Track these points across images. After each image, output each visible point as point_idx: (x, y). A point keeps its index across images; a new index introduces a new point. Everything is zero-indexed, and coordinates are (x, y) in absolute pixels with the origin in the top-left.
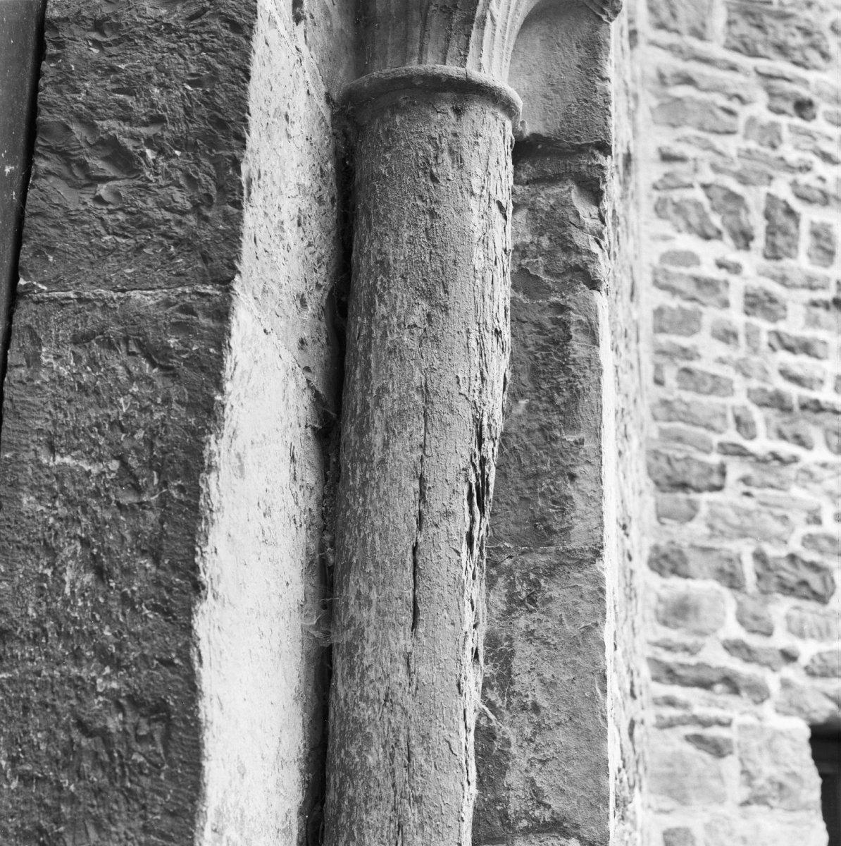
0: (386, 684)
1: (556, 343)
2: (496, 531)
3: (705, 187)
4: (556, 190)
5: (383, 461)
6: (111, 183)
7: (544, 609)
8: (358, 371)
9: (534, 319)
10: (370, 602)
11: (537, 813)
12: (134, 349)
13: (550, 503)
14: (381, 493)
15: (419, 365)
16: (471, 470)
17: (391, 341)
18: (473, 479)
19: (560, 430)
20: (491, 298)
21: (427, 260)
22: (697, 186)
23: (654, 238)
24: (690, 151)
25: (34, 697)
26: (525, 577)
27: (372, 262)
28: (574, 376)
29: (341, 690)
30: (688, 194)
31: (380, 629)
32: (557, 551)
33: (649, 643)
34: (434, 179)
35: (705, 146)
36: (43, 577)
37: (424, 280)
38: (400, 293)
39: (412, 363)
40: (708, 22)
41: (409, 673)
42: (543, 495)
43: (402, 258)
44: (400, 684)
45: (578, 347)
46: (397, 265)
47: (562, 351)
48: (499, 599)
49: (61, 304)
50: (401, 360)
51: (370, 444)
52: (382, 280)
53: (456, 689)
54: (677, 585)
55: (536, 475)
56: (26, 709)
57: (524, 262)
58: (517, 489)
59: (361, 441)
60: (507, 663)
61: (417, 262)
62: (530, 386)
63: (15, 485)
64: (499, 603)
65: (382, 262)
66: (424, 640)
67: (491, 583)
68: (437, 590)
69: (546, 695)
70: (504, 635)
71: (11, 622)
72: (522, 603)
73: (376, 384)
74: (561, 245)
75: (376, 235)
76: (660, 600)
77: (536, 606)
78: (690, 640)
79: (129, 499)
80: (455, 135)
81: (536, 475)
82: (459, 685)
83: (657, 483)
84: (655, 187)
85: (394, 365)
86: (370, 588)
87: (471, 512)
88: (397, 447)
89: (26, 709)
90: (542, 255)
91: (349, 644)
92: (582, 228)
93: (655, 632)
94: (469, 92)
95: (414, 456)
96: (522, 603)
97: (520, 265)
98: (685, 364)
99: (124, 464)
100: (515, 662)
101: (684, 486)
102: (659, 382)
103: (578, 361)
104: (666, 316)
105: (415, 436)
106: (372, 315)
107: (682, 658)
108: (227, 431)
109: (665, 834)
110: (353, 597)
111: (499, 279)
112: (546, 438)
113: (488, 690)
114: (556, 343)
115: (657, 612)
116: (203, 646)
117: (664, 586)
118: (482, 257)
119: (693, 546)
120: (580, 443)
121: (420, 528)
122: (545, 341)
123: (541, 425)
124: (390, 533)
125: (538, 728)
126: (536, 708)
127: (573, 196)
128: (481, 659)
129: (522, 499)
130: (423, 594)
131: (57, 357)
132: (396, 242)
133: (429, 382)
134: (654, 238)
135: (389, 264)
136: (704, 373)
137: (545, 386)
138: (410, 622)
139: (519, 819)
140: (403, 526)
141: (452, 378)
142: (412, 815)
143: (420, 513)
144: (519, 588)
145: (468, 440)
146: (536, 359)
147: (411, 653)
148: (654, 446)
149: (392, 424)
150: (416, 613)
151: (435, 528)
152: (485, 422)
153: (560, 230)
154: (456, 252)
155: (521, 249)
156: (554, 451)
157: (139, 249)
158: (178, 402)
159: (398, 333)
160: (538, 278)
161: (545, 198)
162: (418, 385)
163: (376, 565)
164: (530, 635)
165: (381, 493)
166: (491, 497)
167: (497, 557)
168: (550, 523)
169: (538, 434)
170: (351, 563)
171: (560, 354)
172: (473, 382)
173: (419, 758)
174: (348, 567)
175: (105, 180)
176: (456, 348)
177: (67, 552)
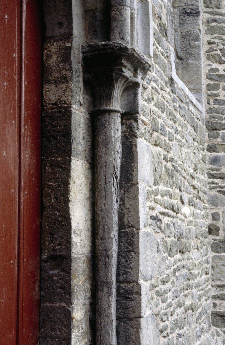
3: (220, 50)
4: (130, 121)
6: (54, 142)
11: (129, 225)
12: (58, 167)
20: (116, 146)
22: (218, 50)
23: (207, 66)
24: (216, 41)
25: (49, 216)
26: (126, 187)
29: (96, 209)
30: (216, 52)
33: (207, 169)
34: (106, 127)
35: (220, 38)
36: (49, 200)
38: (101, 146)
40: (220, 4)
41: (105, 206)
45: (134, 149)
48: (122, 191)
49: (48, 160)
54: (215, 154)
56: (48, 217)
60: (124, 202)
63: (44, 187)
67: (121, 189)
71: (46, 206)
72: (126, 192)
76: (210, 158)
78: (218, 168)
79: (59, 189)
80: (109, 119)
83: (208, 129)
84: (207, 52)
89: (48, 217)
93: (209, 166)
94: (111, 111)
98: (216, 98)
99: (58, 184)
100: (125, 201)
101: (216, 129)
102: (209, 103)
104: (210, 86)
107: (216, 172)
108: (72, 178)
109: (212, 214)
115: (209, 161)
116: (71, 209)
117: (211, 155)
119: (218, 144)
120: (134, 165)
125: (129, 212)
126: (128, 208)
127: (133, 122)
131: (48, 168)
134: (207, 66)
136: (220, 99)
139: (126, 226)
142: (106, 227)
148: (208, 120)
150: (105, 197)
157: (58, 152)
158: (65, 175)
161: (128, 123)
173: (107, 219)
175: (52, 141)
177: (52, 196)
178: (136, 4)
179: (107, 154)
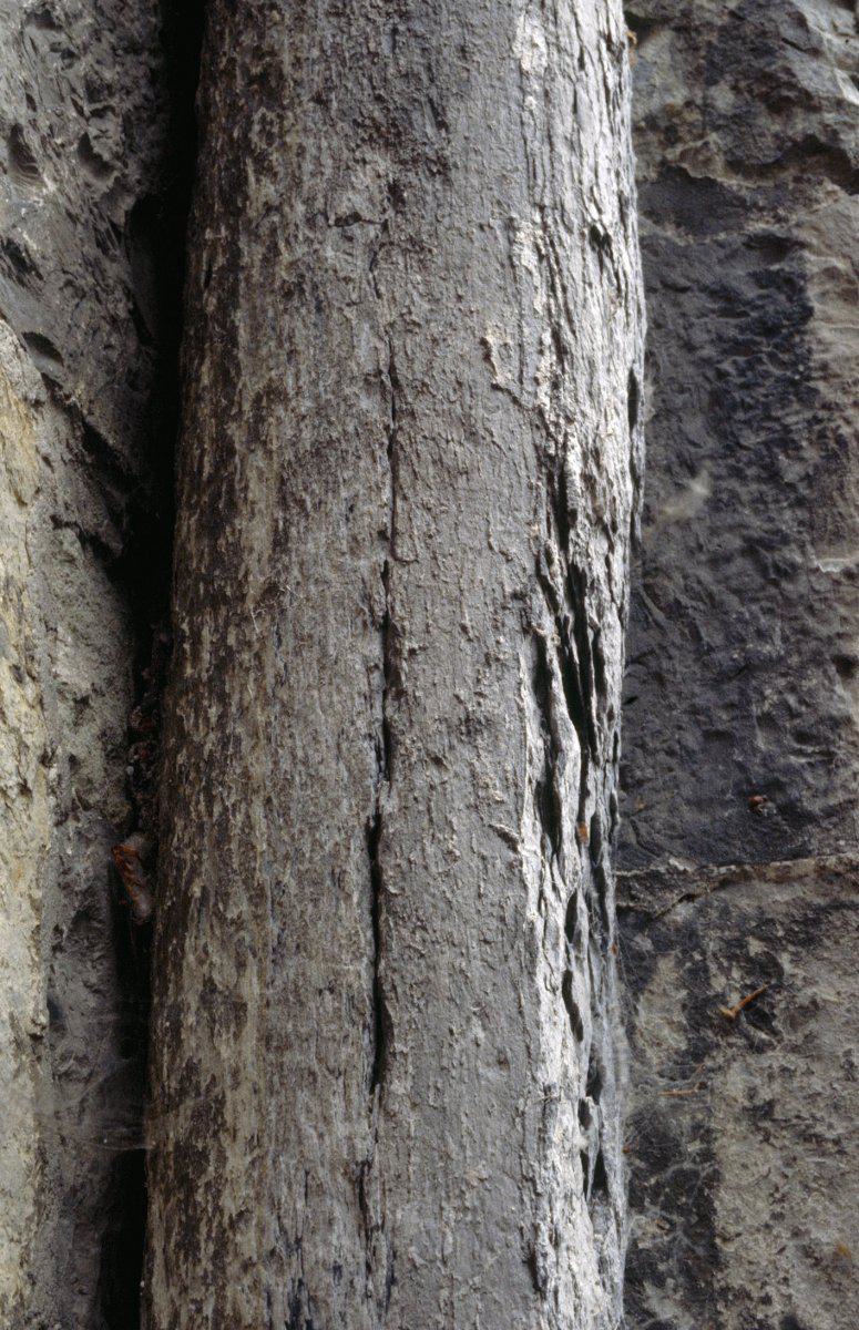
0: (294, 1270)
1: (770, 330)
2: (643, 828)
5: (272, 590)
7: (797, 1038)
8: (204, 369)
9: (708, 280)
10: (239, 1008)
13: (789, 741)
14: (270, 680)
15: (370, 315)
16: (539, 600)
17: (293, 264)
18: (548, 628)
19: (802, 547)
20: (574, 146)
21: (385, 48)
26: (734, 950)
27: (240, 83)
28: (826, 406)
31: (272, 1091)
32: (821, 870)
37: (379, 99)
39: (350, 313)
41: (366, 1230)
42: (767, 721)
43: (315, 53)
44: (337, 1269)
46: (302, 74)
47: (790, 349)
48: (663, 1022)
50: (319, 309)
51: (237, 550)
52: (263, 117)
53: (523, 1275)
55: (746, 670)
57: (672, 154)
58: (694, 711)
59: (214, 548)
60: (705, 1213)
61: (356, 57)
62: (711, 444)
64: (666, 1032)
65: (262, 78)
66: (411, 1119)
67: (636, 973)
68: (447, 956)
69: (823, 1294)
70: (686, 1120)
72: (728, 1026)
73: (250, 384)
74: (764, 98)
75: (250, 15)
77: (774, 1032)
81: (746, 670)
82: (531, 1262)
85: (301, 325)
86: (241, 966)
87: (548, 725)
88: (313, 543)
90: (717, 128)
91: (183, 1151)
92: (815, 52)
95: (363, 564)
96: (728, 1026)
97: (664, 163)
100: (724, 1200)
103: (835, 367)
105: (362, 507)
106: (241, 211)
110: (193, 1000)
111: (594, 106)
112: (763, 570)
113: (649, 1289)
114: (770, 330)
118: (540, 41)
121: (387, 772)
122: (742, 330)
123: (747, 539)
124: (296, 793)
128: (617, 1187)
129: (712, 736)
130: (404, 972)
132: (300, 18)
133: (399, 361)
135: (281, 76)
137: (751, 439)
138: (364, 1065)
140: (334, 770)
141: (464, 345)
143: (386, 726)
144: (719, 983)
145: (524, 515)
146: (722, 375)
147: (368, 1164)
149: (296, 485)
150: (382, 1031)
151: (432, 771)
152: (575, 464)
153: (759, 63)
154: (465, 25)
155: (663, 124)
156: (788, 602)
159: (308, 241)
160: (711, 183)
162: (369, 368)
163: (257, 896)
164: (760, 1114)
165: (270, 680)
166: (615, 701)
167: (648, 901)
168: (793, 793)
169: (740, 563)
170: (187, 900)
171: (785, 357)
172: (532, 359)
174: (179, 921)
176: (476, 266)
178: (855, 898)
179: (416, 245)
